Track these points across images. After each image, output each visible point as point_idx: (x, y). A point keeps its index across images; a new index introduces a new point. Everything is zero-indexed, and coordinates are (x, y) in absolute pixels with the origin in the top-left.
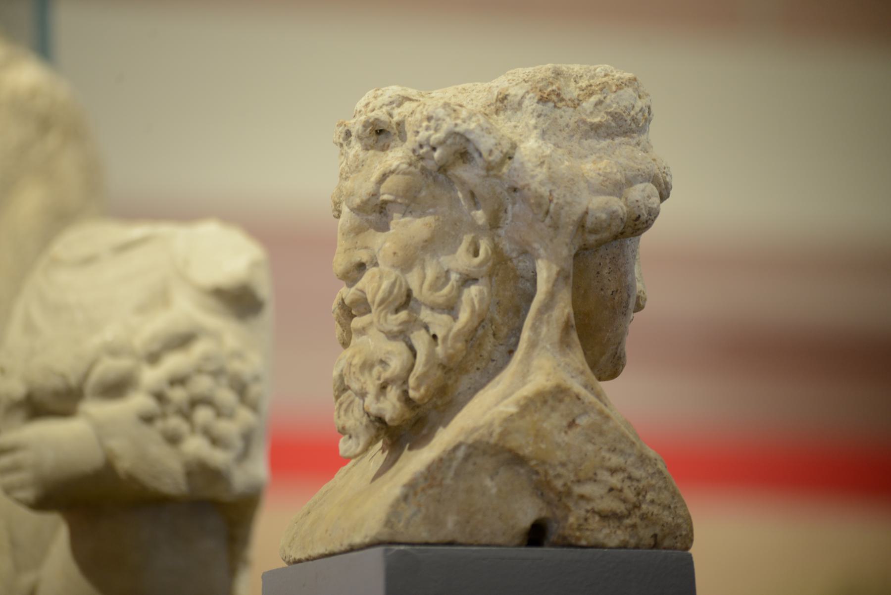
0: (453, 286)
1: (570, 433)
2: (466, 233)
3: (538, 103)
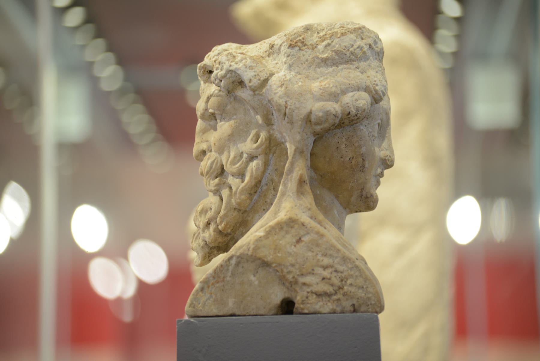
0: (243, 162)
1: (297, 246)
2: (253, 129)
3: (288, 48)
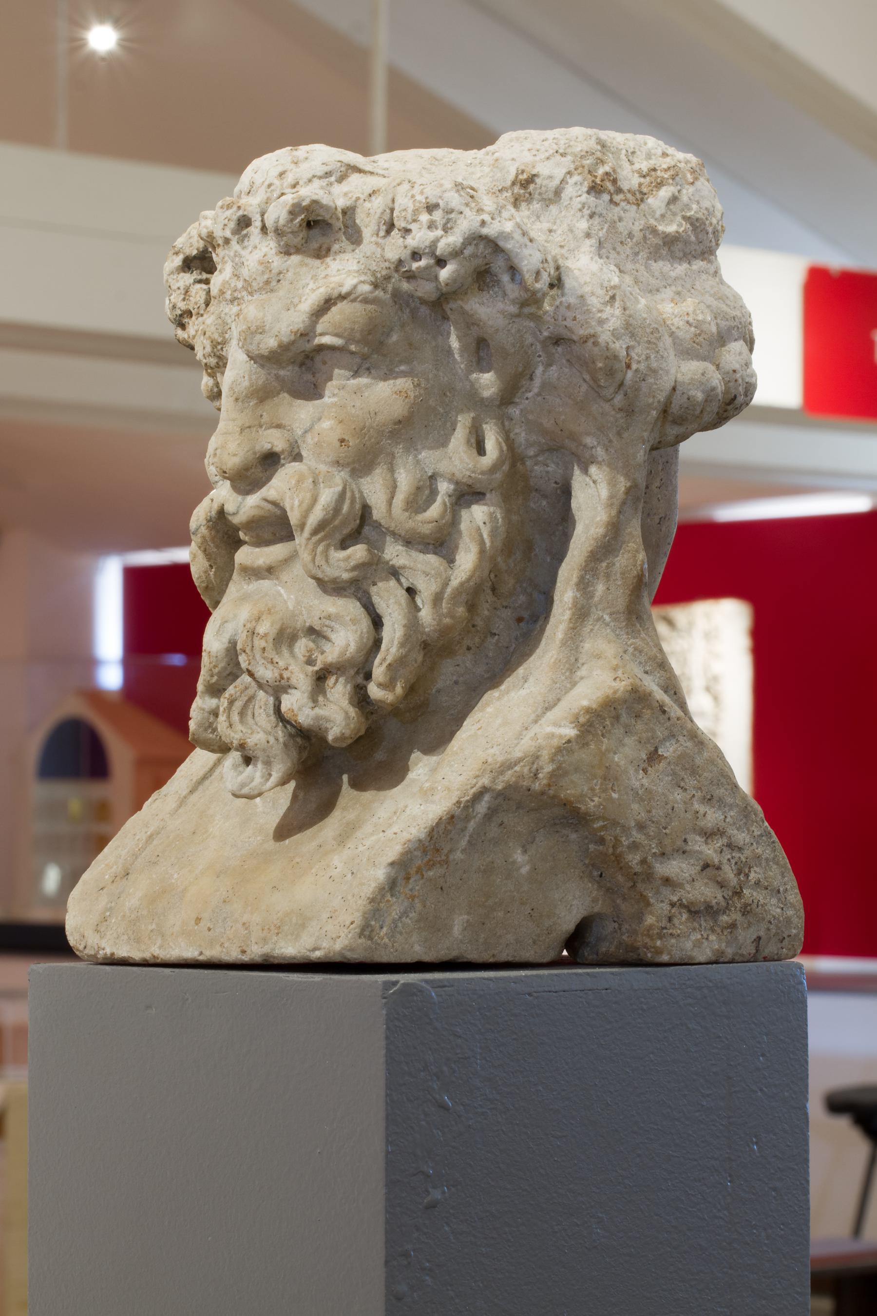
2: (461, 411)
3: (588, 193)
